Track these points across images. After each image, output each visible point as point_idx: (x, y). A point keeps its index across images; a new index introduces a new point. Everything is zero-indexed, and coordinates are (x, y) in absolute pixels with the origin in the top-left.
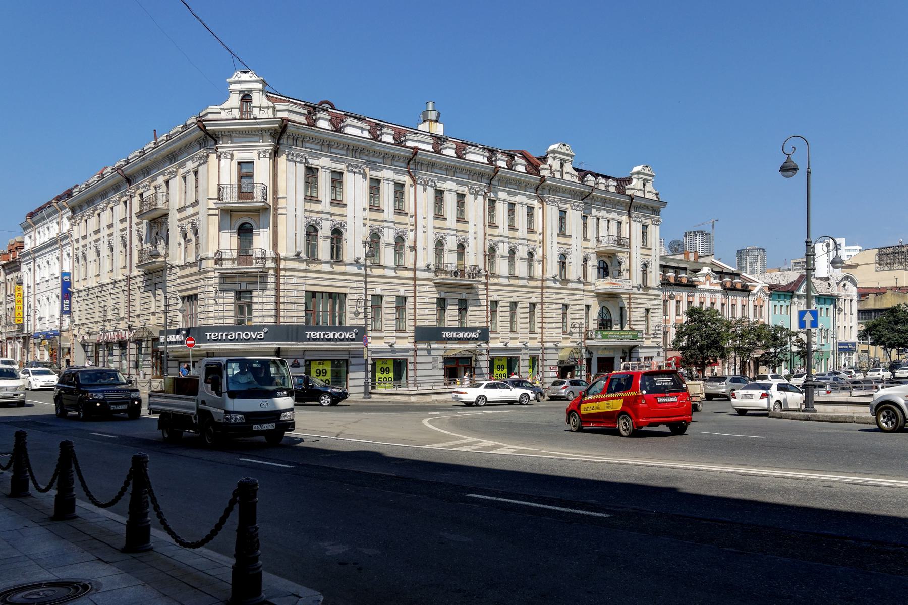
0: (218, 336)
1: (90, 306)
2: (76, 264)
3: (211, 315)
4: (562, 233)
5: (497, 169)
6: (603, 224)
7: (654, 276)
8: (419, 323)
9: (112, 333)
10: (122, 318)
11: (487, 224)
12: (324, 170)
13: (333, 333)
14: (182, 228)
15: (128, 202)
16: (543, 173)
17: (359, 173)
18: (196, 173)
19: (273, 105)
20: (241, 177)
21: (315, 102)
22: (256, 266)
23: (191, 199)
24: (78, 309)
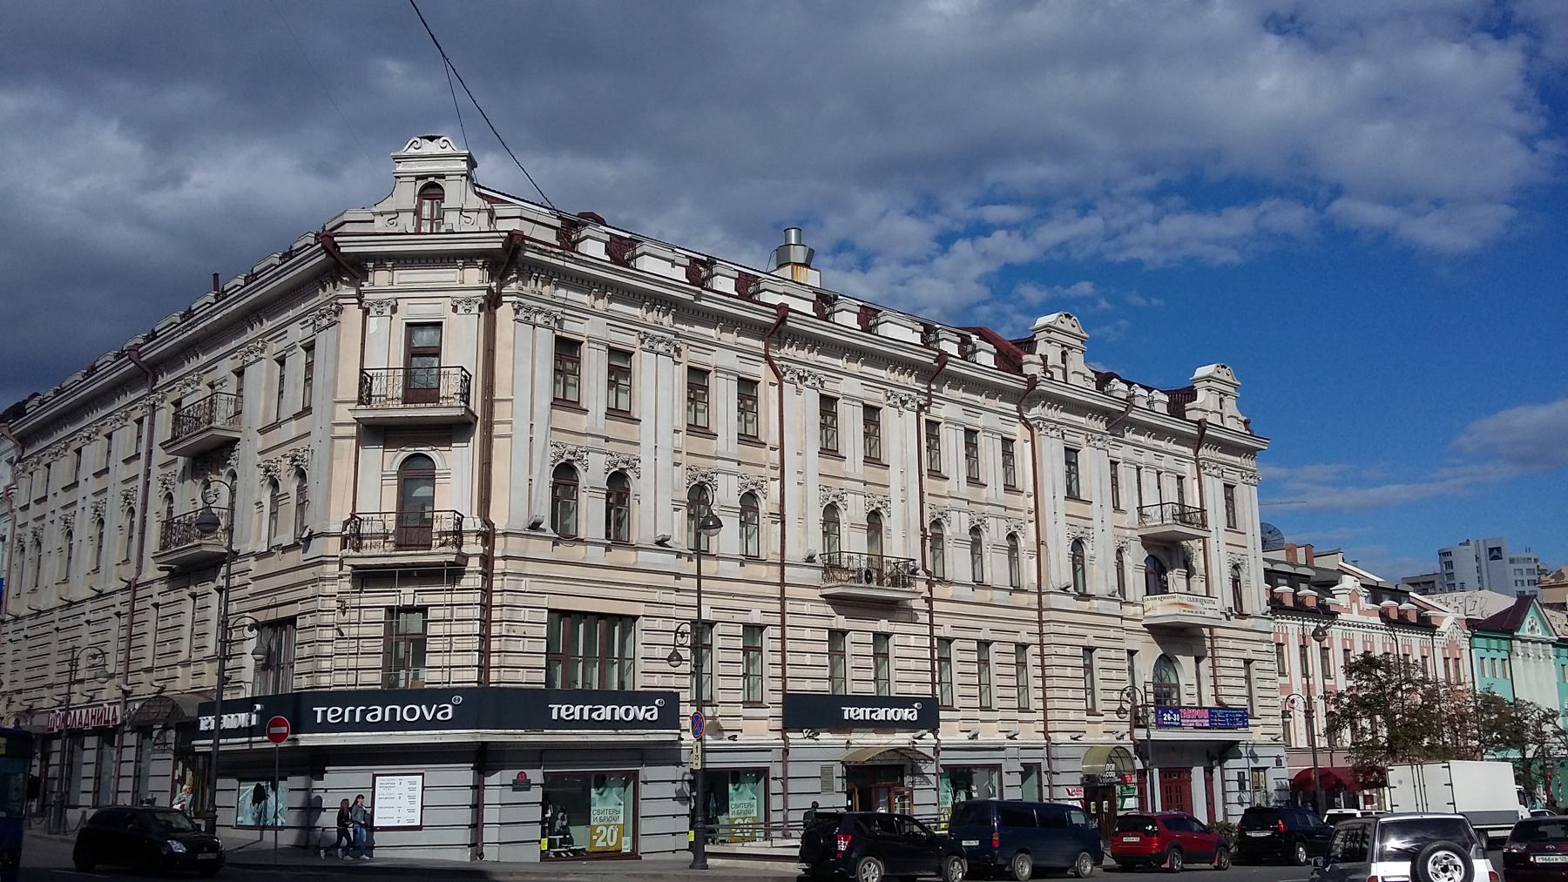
0: (573, 714)
1: (38, 651)
2: (17, 560)
3: (326, 664)
4: (1072, 495)
5: (943, 357)
6: (1149, 478)
7: (1255, 592)
8: (792, 685)
9: (84, 711)
10: (112, 676)
11: (925, 472)
12: (595, 346)
13: (609, 708)
14: (268, 470)
15: (146, 420)
16: (1027, 369)
17: (667, 354)
18: (310, 348)
19: (489, 207)
20: (412, 352)
21: (573, 211)
22: (439, 554)
23: (294, 402)
24: (12, 657)
